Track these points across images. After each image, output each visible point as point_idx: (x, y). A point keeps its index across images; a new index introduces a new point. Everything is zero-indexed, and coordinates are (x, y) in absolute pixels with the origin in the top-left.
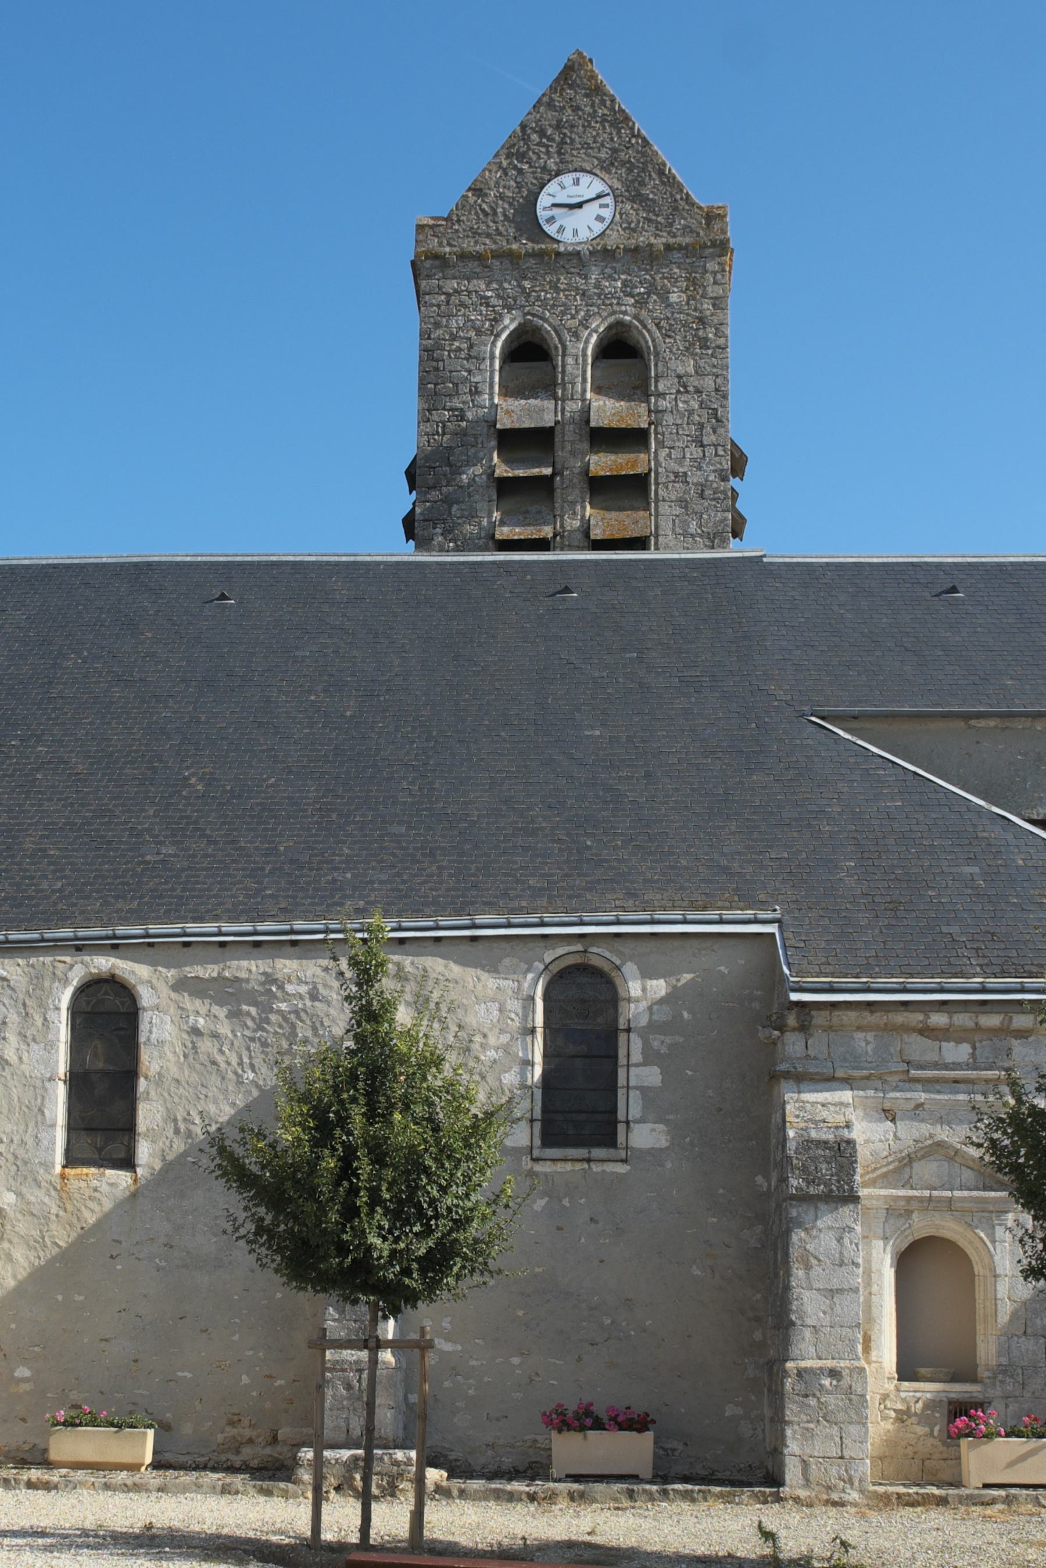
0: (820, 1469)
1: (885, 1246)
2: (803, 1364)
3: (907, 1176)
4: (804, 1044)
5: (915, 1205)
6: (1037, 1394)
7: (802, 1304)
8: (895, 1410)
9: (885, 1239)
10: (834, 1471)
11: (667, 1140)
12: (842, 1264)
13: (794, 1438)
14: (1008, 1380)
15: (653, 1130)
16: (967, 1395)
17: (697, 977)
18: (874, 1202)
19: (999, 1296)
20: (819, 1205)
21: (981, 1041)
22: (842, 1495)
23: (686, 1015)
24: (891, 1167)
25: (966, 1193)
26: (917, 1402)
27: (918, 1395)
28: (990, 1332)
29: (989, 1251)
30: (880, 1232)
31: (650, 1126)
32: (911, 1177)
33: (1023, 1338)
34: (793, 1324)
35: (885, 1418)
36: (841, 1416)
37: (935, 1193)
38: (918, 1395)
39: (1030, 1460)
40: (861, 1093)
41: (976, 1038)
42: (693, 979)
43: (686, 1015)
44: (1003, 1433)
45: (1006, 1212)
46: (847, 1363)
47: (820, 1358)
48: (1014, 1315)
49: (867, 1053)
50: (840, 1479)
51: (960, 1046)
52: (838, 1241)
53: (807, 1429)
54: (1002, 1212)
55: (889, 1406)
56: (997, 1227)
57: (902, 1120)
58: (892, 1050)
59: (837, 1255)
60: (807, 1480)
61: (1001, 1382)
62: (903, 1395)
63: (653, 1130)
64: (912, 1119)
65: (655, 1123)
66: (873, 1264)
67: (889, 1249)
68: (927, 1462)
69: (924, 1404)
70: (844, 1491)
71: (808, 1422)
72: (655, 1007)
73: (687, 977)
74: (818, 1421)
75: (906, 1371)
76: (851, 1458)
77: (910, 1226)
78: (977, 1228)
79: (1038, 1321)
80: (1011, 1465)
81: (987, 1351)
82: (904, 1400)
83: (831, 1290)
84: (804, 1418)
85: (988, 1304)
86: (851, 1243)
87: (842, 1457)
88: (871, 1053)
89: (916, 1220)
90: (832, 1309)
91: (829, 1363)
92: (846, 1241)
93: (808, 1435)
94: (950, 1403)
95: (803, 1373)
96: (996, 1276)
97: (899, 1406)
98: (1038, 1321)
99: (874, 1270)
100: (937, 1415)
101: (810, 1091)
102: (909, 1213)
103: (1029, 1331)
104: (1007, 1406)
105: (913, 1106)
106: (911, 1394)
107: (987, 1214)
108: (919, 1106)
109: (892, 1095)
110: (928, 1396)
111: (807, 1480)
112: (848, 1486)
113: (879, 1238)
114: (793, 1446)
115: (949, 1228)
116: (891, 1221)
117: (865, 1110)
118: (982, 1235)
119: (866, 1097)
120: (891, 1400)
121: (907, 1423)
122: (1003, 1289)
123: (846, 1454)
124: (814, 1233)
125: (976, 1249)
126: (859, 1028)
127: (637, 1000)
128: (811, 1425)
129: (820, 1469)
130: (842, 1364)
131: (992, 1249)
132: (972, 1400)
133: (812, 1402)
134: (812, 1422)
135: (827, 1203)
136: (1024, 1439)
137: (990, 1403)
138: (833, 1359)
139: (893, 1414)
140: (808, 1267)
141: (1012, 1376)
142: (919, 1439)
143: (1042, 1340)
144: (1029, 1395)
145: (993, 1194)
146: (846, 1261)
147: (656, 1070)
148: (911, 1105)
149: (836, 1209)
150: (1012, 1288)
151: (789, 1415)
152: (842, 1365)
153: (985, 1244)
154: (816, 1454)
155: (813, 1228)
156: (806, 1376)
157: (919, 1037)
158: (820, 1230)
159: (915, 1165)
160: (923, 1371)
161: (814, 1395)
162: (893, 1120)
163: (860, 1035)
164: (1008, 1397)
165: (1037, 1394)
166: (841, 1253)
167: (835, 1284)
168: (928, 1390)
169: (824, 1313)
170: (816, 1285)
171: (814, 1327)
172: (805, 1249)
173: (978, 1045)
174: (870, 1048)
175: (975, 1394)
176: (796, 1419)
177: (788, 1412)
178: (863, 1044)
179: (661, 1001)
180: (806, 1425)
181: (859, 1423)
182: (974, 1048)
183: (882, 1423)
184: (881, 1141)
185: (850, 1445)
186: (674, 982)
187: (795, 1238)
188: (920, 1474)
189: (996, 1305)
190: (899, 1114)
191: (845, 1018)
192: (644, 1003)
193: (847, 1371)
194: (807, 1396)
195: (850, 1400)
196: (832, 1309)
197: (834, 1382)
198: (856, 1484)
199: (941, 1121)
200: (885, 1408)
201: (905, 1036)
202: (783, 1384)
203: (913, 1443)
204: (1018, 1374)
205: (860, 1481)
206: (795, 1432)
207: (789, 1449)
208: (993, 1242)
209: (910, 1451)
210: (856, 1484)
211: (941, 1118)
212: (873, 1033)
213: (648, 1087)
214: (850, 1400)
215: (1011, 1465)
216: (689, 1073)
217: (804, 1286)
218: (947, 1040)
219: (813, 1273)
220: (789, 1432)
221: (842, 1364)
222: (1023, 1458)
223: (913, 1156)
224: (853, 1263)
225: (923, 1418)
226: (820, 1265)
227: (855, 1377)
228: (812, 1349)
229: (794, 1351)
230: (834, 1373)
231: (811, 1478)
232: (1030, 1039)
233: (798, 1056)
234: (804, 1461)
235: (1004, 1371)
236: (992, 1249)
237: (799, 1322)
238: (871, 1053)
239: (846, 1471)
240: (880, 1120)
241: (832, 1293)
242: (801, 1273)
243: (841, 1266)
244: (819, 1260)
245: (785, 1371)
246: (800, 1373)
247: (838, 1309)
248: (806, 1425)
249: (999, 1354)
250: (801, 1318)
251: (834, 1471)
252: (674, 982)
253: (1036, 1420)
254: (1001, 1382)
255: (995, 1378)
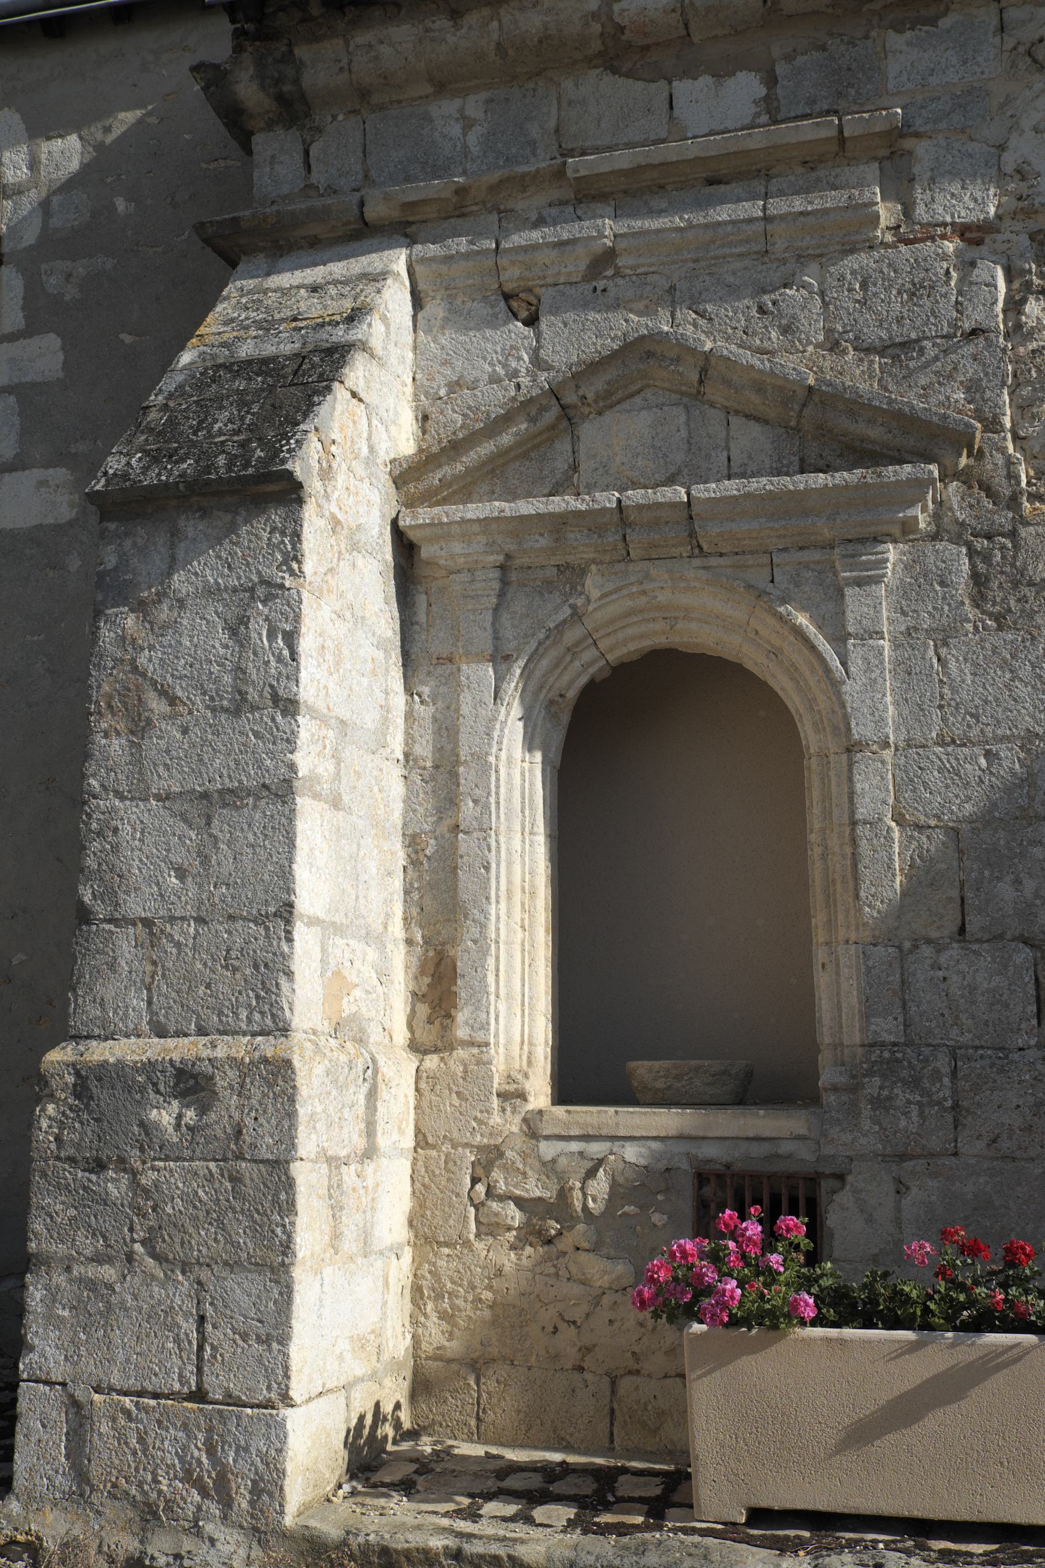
0: (122, 1438)
1: (500, 679)
2: (99, 1052)
3: (561, 465)
4: (298, 158)
5: (581, 548)
6: (1006, 1145)
7: (116, 848)
8: (519, 1202)
9: (501, 659)
10: (168, 1446)
11: (71, 505)
12: (240, 706)
13: (51, 1319)
14: (901, 1095)
15: (42, 483)
16: (758, 1151)
17: (149, 114)
18: (458, 547)
19: (862, 812)
20: (182, 523)
21: (789, 58)
22: (188, 1544)
23: (121, 205)
24: (506, 439)
25: (732, 487)
26: (591, 1173)
27: (596, 1149)
28: (842, 934)
29: (828, 670)
30: (483, 639)
31: (37, 473)
32: (575, 467)
33: (955, 951)
34: (84, 915)
35: (489, 1228)
36: (204, 1240)
37: (635, 496)
38: (596, 1149)
39: (932, 1422)
40: (433, 249)
41: (776, 51)
42: (140, 122)
43: (121, 205)
44: (810, 1313)
45: (877, 540)
46: (239, 1047)
47: (161, 1032)
48: (922, 878)
49: (466, 151)
50: (189, 1477)
51: (731, 83)
52: (233, 632)
53: (92, 1285)
54: (862, 540)
55: (502, 1187)
56: (849, 592)
57: (555, 311)
58: (534, 132)
59: (227, 679)
60: (81, 1476)
61: (877, 1103)
62: (548, 1150)
63: (42, 483)
64: (585, 305)
65: (47, 466)
66: (463, 737)
67: (512, 686)
68: (626, 1384)
69: (614, 1185)
70: (196, 1530)
71: (98, 1259)
72: (55, 199)
73: (129, 117)
74: (130, 1258)
75: (580, 1075)
76: (231, 1400)
77: (577, 616)
78: (784, 601)
79: (1006, 890)
80: (860, 1435)
81: (840, 1002)
82: (549, 1167)
83: (205, 795)
84: (88, 1245)
85: (834, 842)
86: (272, 635)
87: (199, 1396)
88: (475, 149)
89: (595, 594)
90: (205, 860)
91: (180, 1049)
92: (258, 630)
93: (95, 1306)
94: (701, 1178)
95: (92, 1084)
96: (852, 748)
97: (534, 1189)
98: (1006, 890)
99: (464, 753)
100: (657, 1218)
101: (292, 269)
102: (571, 575)
103: (975, 923)
104: (901, 1188)
105: (583, 266)
106: (574, 1146)
107: (816, 555)
108: (604, 261)
109: (518, 239)
110: (631, 1153)
111: (81, 1476)
112: (214, 1508)
113: (479, 657)
114: (45, 1350)
115: (704, 614)
116: (519, 604)
117: (450, 299)
118: (802, 620)
119: (448, 259)
120: (509, 1169)
121: (561, 1245)
122: (875, 787)
123: (215, 1384)
124: (164, 612)
125: (792, 671)
126: (443, 85)
127: (18, 191)
128: (108, 1273)
129: (122, 1438)
130: (224, 1048)
131: (835, 663)
132: (779, 1167)
133: (115, 1186)
134: (109, 1260)
135: (204, 513)
136: (908, 1335)
137: (841, 1177)
138: (202, 1032)
139: (514, 1215)
140: (140, 726)
141: (914, 1083)
142: (597, 1301)
143: (1023, 955)
144: (980, 1146)
145: (820, 479)
146: (253, 695)
147: (51, 342)
148: (576, 264)
149: (232, 529)
150: (907, 783)
151: (40, 1238)
152: (220, 1053)
153: (813, 648)
154: (116, 1379)
155: (161, 596)
156: (101, 1094)
157: (608, 79)
158: (181, 603)
159: (588, 431)
160: (642, 1069)
161: (122, 1163)
162: (531, 321)
163: (446, 108)
164: (902, 1157)
165: (1006, 1145)
166: (239, 670)
167: (219, 773)
168: (638, 1132)
169: (181, 873)
170: (163, 782)
171: (147, 923)
172: (135, 669)
173: (781, 69)
174: (472, 139)
175: (785, 1148)
176: (62, 1249)
177: (37, 1225)
178: (456, 130)
179: (74, 182)
180: (91, 1271)
181: (260, 1266)
182: (771, 80)
183: (479, 1246)
184: (495, 379)
185: (227, 1348)
186: (99, 136)
187: (107, 635)
188: (603, 1426)
189: (854, 842)
190: (547, 295)
191: (385, 50)
192: (33, 193)
193: (232, 1074)
194: (99, 1166)
195: (235, 1179)
196: (205, 860)
197: (190, 1115)
198: (242, 1503)
199: (671, 297)
200: (489, 1193)
201: (568, 84)
202: (30, 1124)
203: (578, 1314)
204: (936, 1075)
205: (256, 1491)
206: (53, 1295)
207: (34, 1357)
208: (839, 639)
209: (567, 1340)
210: (242, 1503)
211: (672, 289)
212: (483, 95)
213: (34, 385)
214: (235, 1179)
215: (860, 1435)
216: (127, 338)
217: (124, 787)
218: (690, 73)
219: (153, 745)
220: (35, 1296)
221: (224, 1048)
222: (905, 1410)
223: (570, 398)
224: (276, 699)
225: (611, 1230)
226: (172, 717)
227: (256, 1093)
228: (137, 1002)
229: (85, 1011)
230: (191, 1084)
231: (95, 1472)
232: (945, 23)
233: (285, 190)
234: (75, 1404)
235: (887, 1063)
236: (835, 663)
237: (101, 910)
238: (475, 149)
239: (211, 1451)
240: (493, 322)
241: (208, 804)
242: (117, 747)
243: (236, 712)
244: (173, 701)
245: (42, 1080)
246: (86, 1082)
247: (224, 861)
248: (91, 1271)
249: (869, 1011)
250: (109, 895)
251: (168, 1446)
252: (99, 136)
253: (972, 1249)
254: (877, 1103)
255: (855, 1089)
